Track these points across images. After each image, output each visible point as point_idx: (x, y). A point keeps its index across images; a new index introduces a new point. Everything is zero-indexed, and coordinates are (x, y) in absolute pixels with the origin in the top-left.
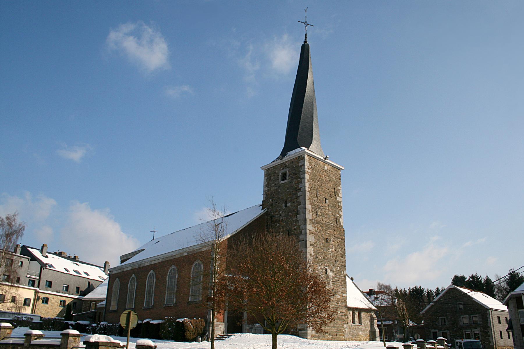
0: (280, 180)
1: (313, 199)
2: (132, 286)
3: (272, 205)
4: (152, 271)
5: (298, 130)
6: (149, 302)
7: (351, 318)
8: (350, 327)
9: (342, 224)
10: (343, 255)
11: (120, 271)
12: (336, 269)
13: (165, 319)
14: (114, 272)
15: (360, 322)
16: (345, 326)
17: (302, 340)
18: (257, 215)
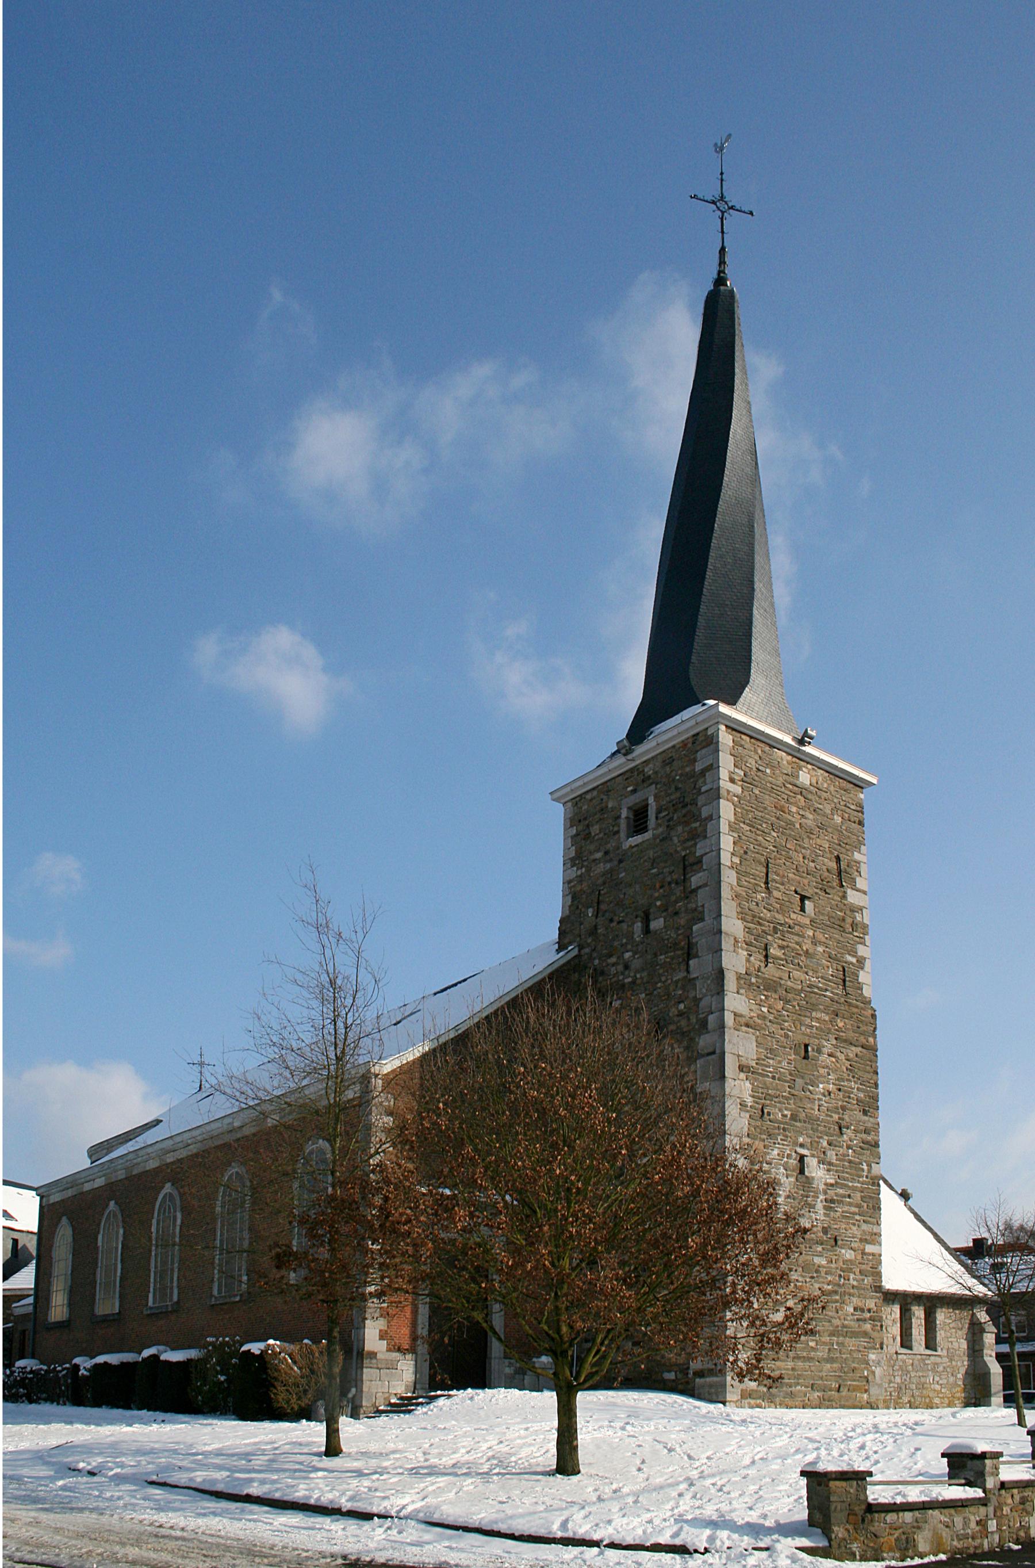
0: (623, 835)
1: (749, 899)
2: (110, 1239)
3: (593, 931)
4: (168, 1185)
5: (698, 635)
6: (163, 1291)
7: (896, 1330)
8: (891, 1362)
9: (867, 992)
10: (870, 1106)
11: (70, 1193)
12: (842, 1158)
13: (205, 1346)
14: (55, 1198)
15: (930, 1343)
16: (872, 1356)
17: (705, 1407)
18: (539, 968)
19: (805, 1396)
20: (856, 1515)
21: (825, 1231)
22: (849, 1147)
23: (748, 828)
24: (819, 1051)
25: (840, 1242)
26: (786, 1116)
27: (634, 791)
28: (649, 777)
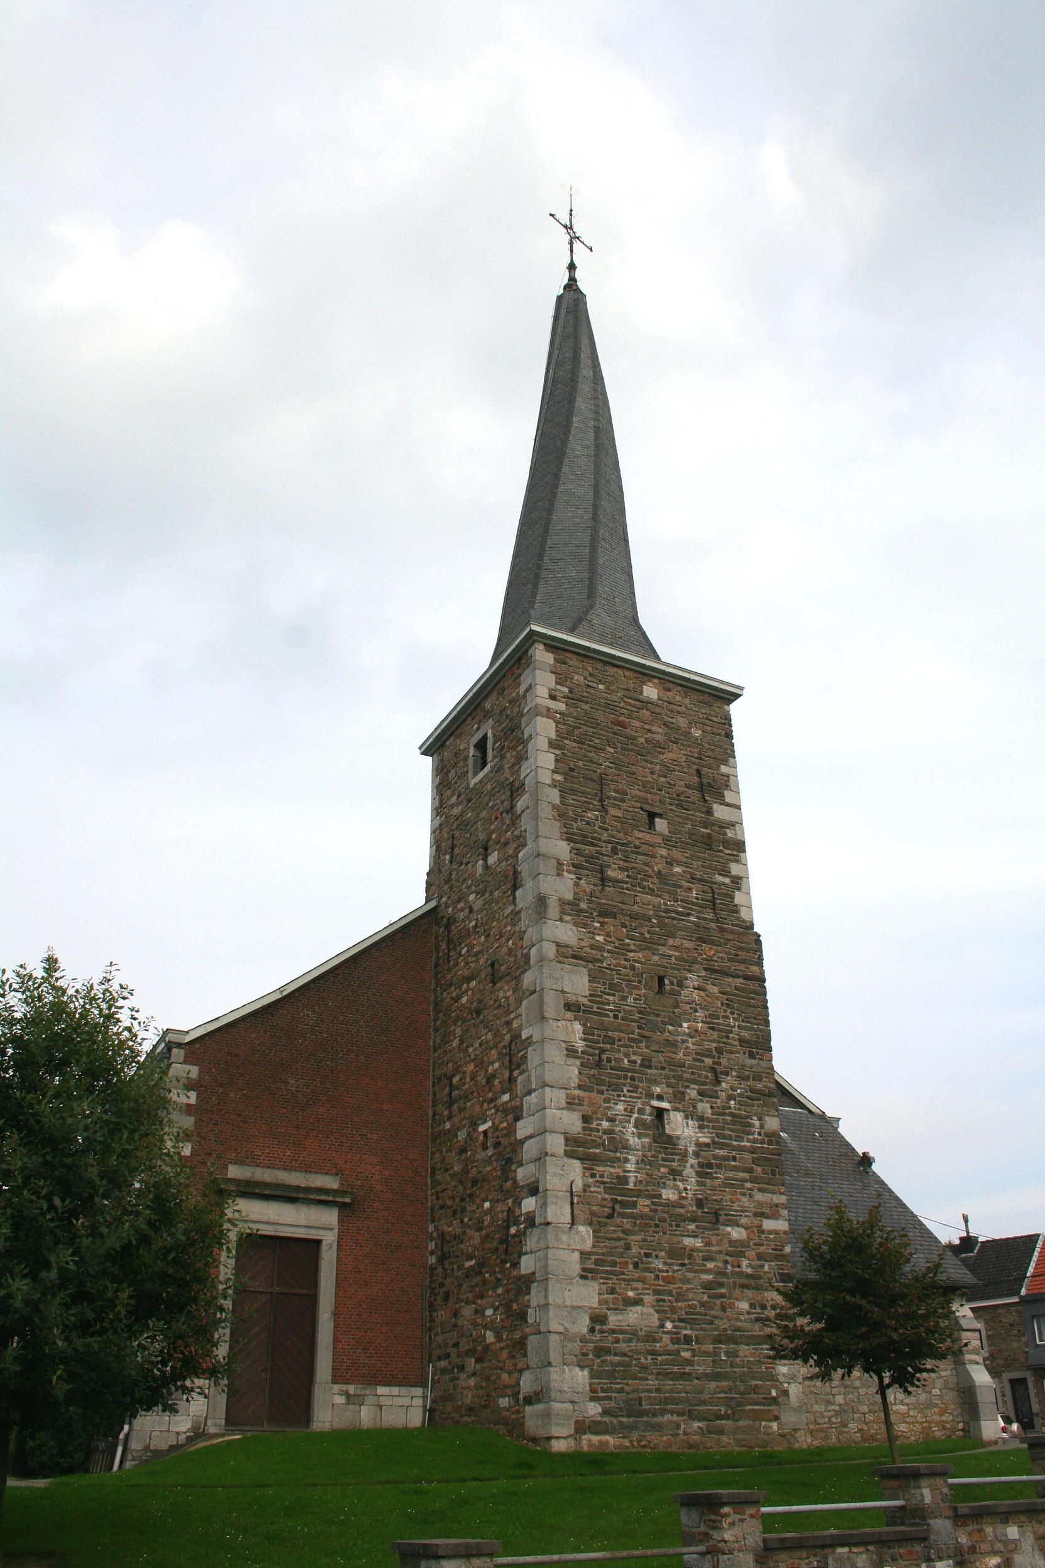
12: (720, 1112)
21: (700, 1203)
22: (730, 1098)
23: (575, 744)
24: (681, 985)
25: (722, 1218)
26: (635, 1062)
27: (478, 729)
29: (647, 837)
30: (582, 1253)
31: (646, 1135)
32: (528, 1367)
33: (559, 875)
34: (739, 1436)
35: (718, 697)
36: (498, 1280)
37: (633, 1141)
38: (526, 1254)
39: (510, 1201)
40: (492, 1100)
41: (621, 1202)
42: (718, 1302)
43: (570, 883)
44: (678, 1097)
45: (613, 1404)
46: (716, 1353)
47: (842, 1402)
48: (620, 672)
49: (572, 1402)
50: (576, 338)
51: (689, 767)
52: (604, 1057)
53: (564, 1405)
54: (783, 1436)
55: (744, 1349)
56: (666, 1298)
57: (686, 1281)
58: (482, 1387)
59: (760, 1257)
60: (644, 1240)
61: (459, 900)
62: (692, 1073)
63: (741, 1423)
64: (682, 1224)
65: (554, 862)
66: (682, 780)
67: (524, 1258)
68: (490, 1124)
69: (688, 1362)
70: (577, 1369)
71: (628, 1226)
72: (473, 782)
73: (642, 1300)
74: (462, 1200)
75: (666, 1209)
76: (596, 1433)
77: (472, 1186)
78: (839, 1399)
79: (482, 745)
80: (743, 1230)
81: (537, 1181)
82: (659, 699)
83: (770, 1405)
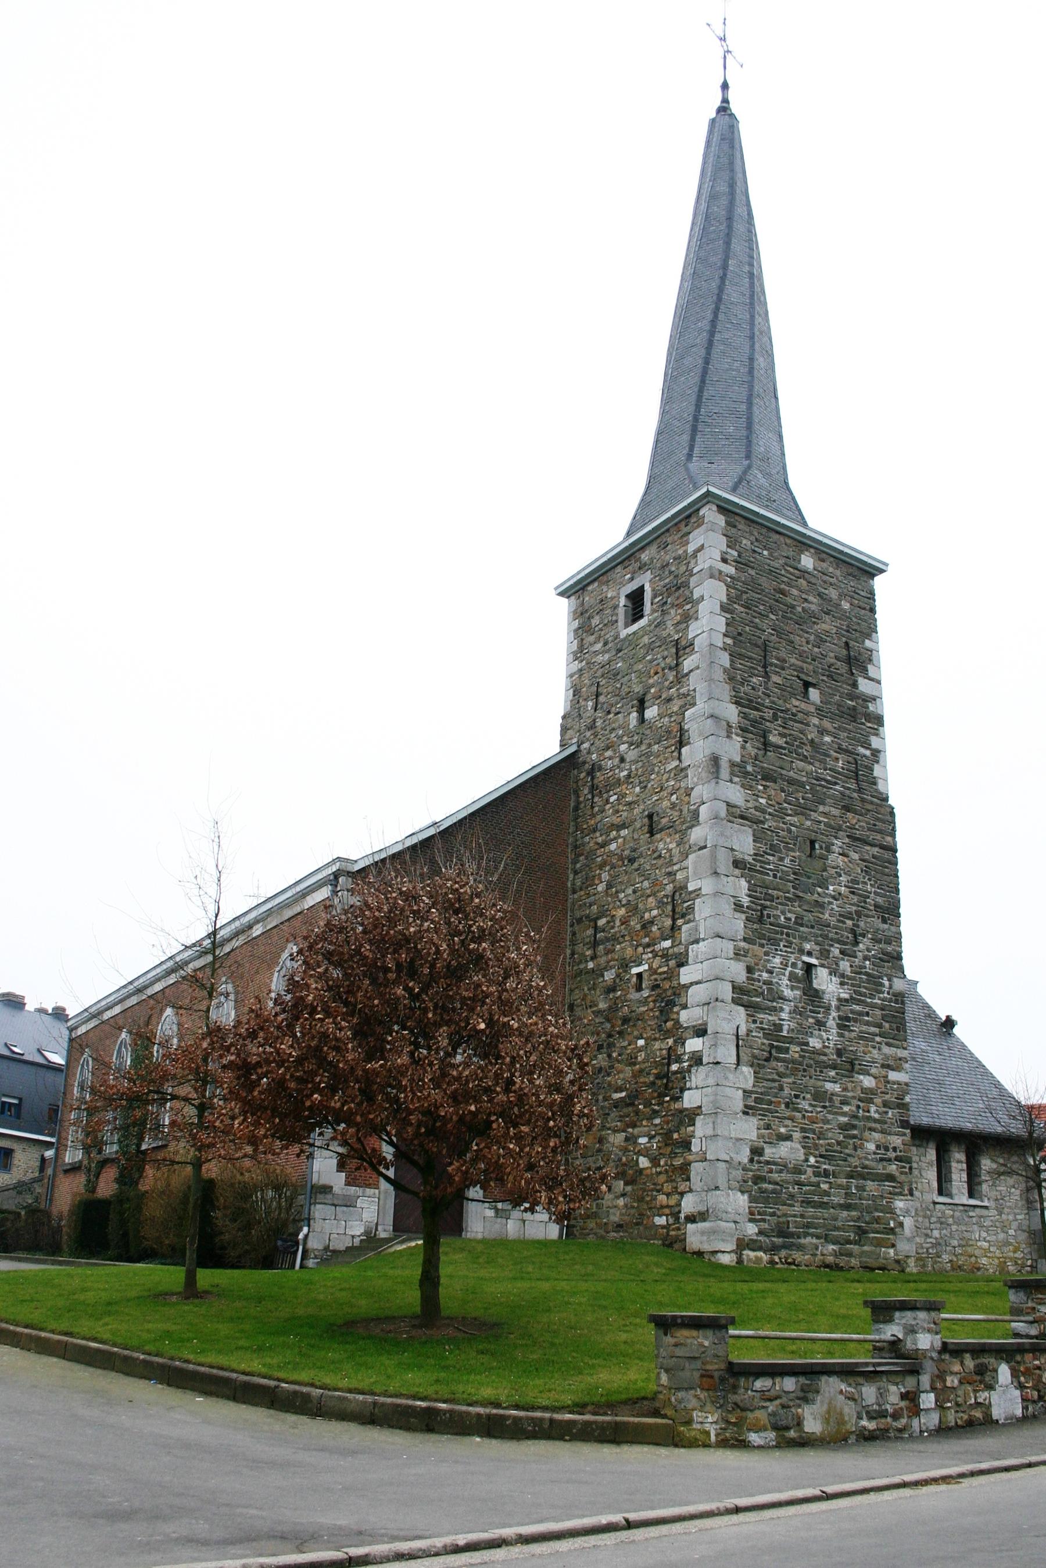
0: (621, 623)
3: (592, 726)
8: (925, 1212)
10: (891, 911)
12: (858, 970)
19: (817, 1249)
20: (712, 1377)
21: (839, 1053)
22: (866, 958)
23: (743, 609)
24: (829, 850)
25: (857, 1067)
26: (790, 919)
27: (632, 579)
28: (645, 564)
29: (803, 706)
30: (745, 1091)
31: (797, 988)
32: (691, 1191)
33: (728, 737)
34: (865, 1259)
35: (862, 571)
36: (655, 1112)
37: (788, 993)
38: (689, 1089)
39: (671, 1041)
40: (648, 945)
41: (777, 1047)
42: (851, 1142)
43: (738, 745)
44: (824, 954)
45: (767, 1226)
46: (848, 1187)
47: (938, 1236)
48: (782, 538)
49: (735, 1222)
50: (732, 170)
51: (839, 639)
52: (765, 913)
53: (728, 1224)
54: (898, 1262)
55: (870, 1185)
56: (811, 1136)
57: (826, 1121)
58: (633, 1207)
59: (885, 1104)
60: (794, 1083)
61: (608, 748)
62: (836, 933)
63: (866, 1248)
64: (825, 1070)
65: (725, 723)
66: (833, 651)
67: (686, 1094)
68: (646, 967)
69: (827, 1193)
70: (739, 1194)
71: (782, 1070)
72: (624, 633)
73: (791, 1136)
74: (610, 1036)
75: (813, 1056)
76: (754, 1250)
77: (623, 1024)
78: (936, 1233)
79: (636, 598)
80: (872, 1079)
81: (706, 1024)
82: (815, 569)
83: (888, 1234)
